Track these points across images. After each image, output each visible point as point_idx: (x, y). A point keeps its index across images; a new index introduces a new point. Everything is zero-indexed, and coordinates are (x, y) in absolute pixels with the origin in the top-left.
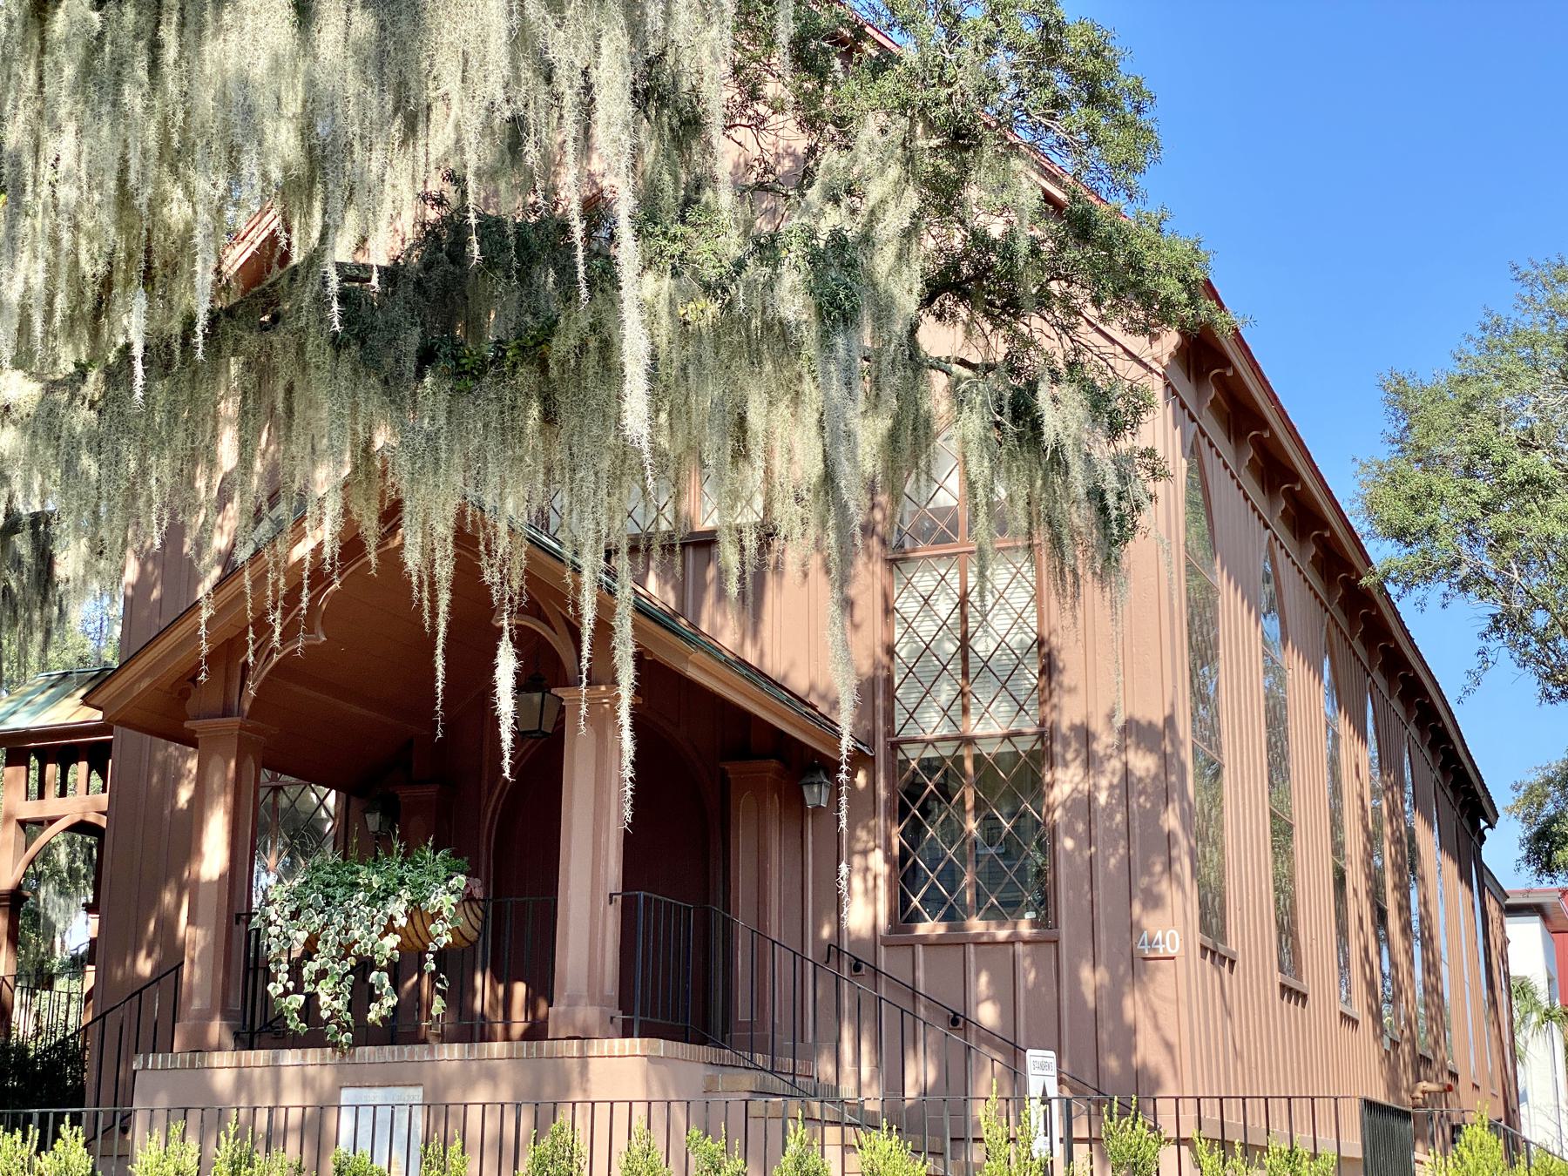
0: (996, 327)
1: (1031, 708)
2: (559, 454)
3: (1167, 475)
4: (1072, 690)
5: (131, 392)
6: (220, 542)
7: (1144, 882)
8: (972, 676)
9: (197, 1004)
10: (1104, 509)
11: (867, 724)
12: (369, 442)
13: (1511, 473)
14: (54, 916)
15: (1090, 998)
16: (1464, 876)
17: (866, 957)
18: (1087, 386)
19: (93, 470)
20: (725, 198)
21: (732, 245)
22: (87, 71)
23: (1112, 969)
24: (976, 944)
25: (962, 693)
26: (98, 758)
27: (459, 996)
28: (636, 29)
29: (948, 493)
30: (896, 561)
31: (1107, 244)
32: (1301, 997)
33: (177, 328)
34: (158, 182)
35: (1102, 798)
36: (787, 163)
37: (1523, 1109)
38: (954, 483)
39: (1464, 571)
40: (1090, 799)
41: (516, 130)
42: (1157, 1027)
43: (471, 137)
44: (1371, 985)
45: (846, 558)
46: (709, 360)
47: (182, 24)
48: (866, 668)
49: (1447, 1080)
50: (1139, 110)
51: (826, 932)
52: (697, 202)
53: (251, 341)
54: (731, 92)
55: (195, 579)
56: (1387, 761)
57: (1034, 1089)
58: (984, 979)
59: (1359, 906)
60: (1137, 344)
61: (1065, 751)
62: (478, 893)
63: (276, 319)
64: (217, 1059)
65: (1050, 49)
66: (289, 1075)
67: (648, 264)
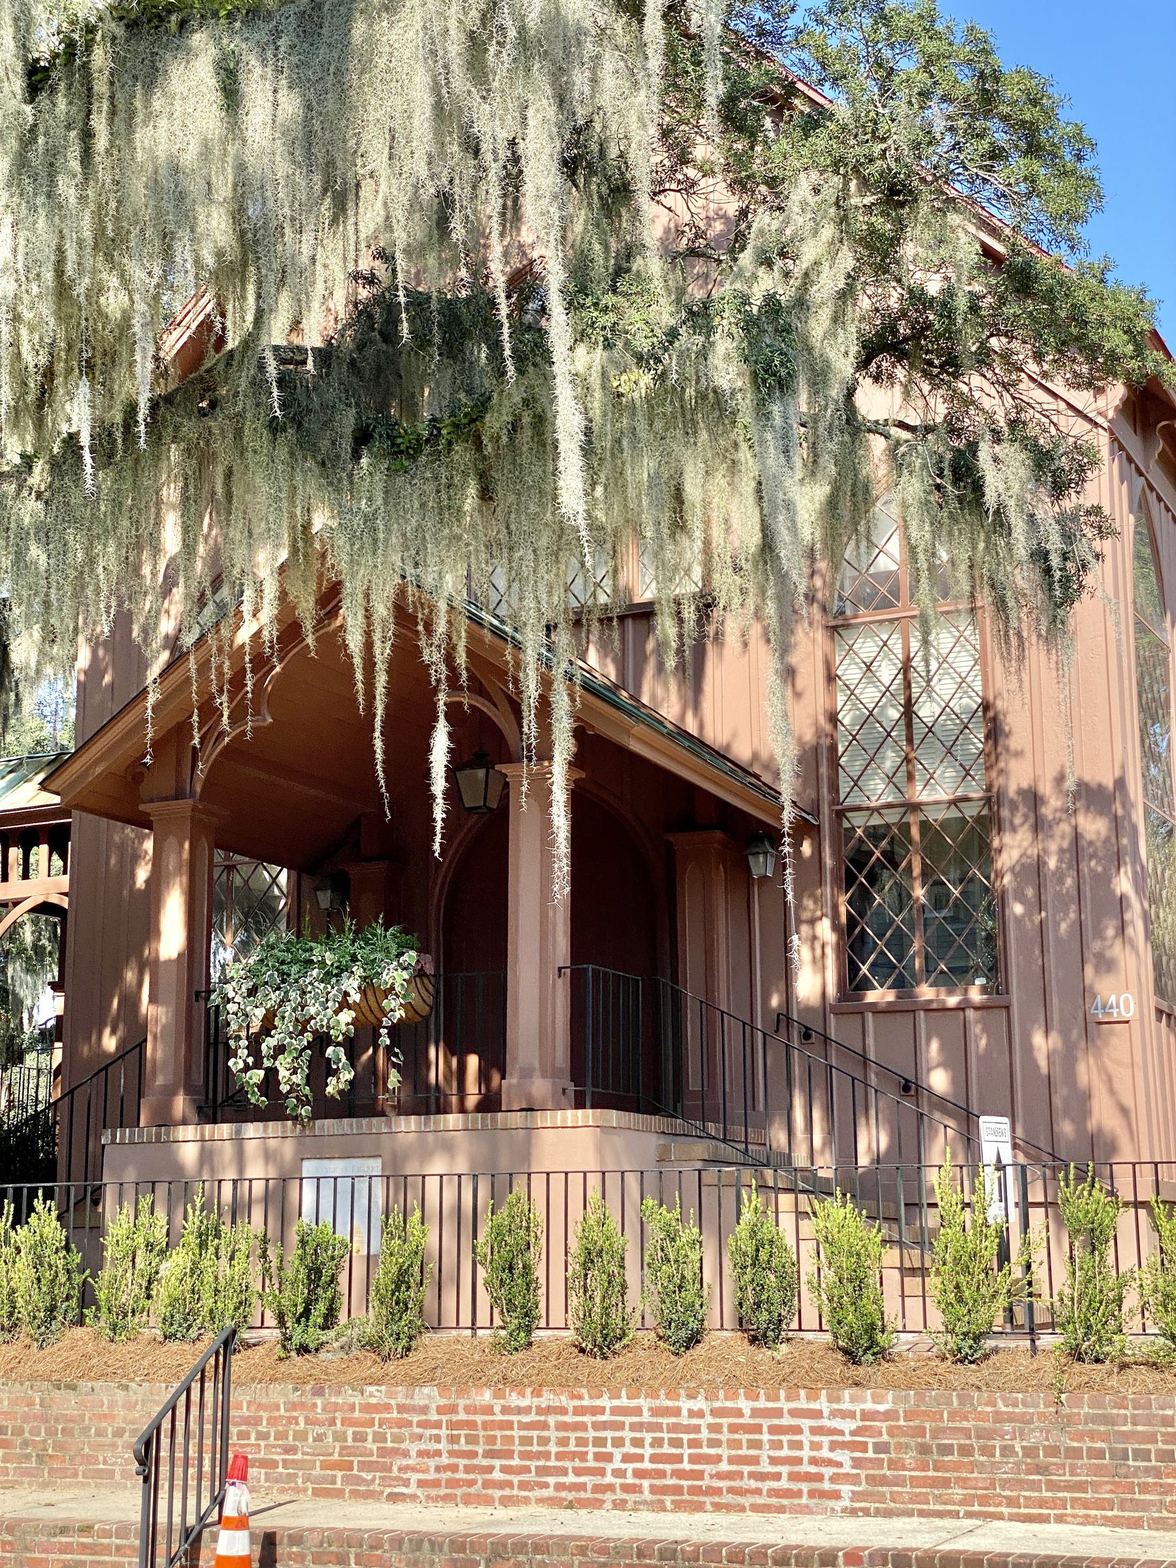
1: (978, 773)
3: (1114, 533)
4: (1019, 754)
6: (167, 626)
7: (1096, 946)
8: (916, 742)
9: (160, 1081)
10: (1048, 571)
11: (811, 793)
12: (307, 526)
14: (22, 992)
15: (1043, 1063)
20: (652, 265)
21: (665, 314)
23: (1065, 1033)
24: (926, 1010)
25: (907, 760)
26: (58, 840)
27: (415, 1068)
30: (838, 626)
31: (1049, 297)
34: (95, 271)
35: (1052, 863)
36: (718, 226)
38: (894, 547)
40: (1040, 863)
42: (1112, 1092)
46: (642, 426)
47: (113, 113)
48: (809, 736)
50: (1079, 158)
51: (775, 1001)
53: (190, 427)
54: (661, 157)
55: (144, 665)
58: (935, 1045)
60: (1082, 398)
61: (1012, 814)
62: (430, 969)
63: (213, 405)
64: (188, 1132)
66: (251, 1147)
67: (581, 336)
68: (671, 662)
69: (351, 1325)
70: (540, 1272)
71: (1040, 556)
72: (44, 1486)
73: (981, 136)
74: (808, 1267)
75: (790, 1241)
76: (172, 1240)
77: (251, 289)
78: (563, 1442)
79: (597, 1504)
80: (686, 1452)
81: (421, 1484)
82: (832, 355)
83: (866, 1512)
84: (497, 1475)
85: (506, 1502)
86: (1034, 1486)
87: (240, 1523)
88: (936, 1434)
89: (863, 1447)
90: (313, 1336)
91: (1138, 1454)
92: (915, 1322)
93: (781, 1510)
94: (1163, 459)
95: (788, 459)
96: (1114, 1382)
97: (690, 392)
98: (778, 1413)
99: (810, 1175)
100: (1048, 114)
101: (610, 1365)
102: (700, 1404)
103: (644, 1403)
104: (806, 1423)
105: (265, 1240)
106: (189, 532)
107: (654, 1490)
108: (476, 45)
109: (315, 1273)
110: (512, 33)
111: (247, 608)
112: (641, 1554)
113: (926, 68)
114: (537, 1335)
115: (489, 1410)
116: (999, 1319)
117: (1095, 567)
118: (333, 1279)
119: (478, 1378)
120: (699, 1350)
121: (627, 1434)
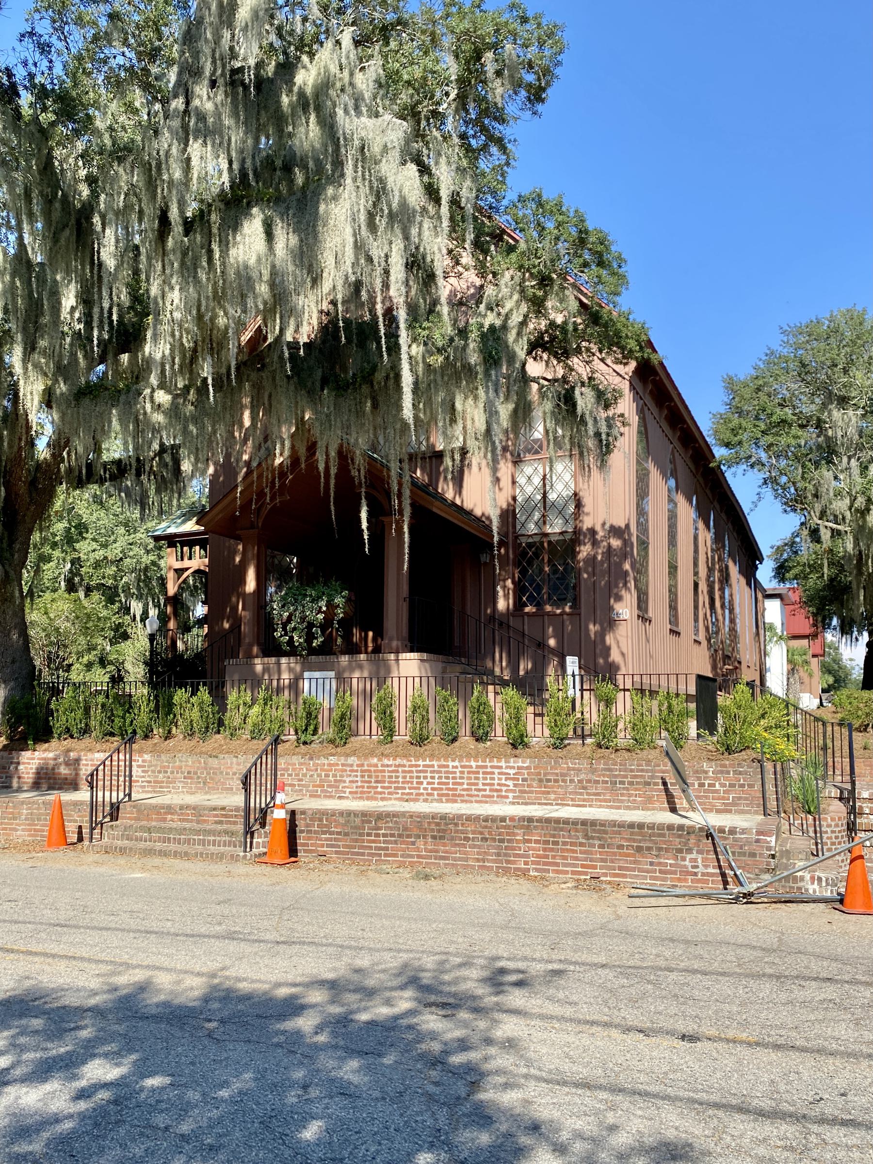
0: (559, 362)
1: (571, 522)
2: (379, 420)
3: (629, 425)
4: (588, 514)
5: (209, 399)
6: (246, 457)
7: (615, 591)
9: (247, 640)
10: (601, 441)
11: (505, 529)
12: (303, 417)
13: (774, 418)
14: (189, 604)
15: (593, 636)
16: (749, 584)
17: (505, 621)
18: (595, 388)
19: (195, 431)
20: (445, 310)
21: (449, 330)
22: (183, 264)
25: (544, 516)
26: (203, 544)
27: (347, 636)
28: (407, 237)
29: (538, 433)
30: (517, 462)
31: (606, 326)
32: (678, 634)
33: (224, 370)
34: (214, 309)
35: (599, 557)
36: (472, 291)
37: (768, 674)
38: (541, 428)
39: (753, 460)
41: (357, 286)
42: (619, 647)
43: (339, 288)
44: (707, 628)
45: (495, 461)
46: (439, 379)
47: (220, 241)
48: (505, 506)
49: (736, 664)
50: (620, 267)
51: (489, 611)
52: (434, 311)
53: (254, 376)
54: (448, 261)
55: (236, 474)
56: (718, 539)
57: (569, 671)
58: (551, 629)
59: (704, 598)
60: (619, 368)
62: (353, 598)
63: (263, 366)
64: (258, 661)
65: (581, 243)
66: (284, 667)
67: (414, 340)
68: (449, 477)
69: (323, 733)
70: (396, 715)
71: (598, 434)
72: (206, 793)
73: (580, 256)
74: (498, 713)
75: (492, 703)
76: (254, 701)
77: (278, 316)
78: (404, 777)
79: (416, 800)
80: (451, 781)
81: (350, 793)
82: (517, 350)
83: (518, 803)
84: (379, 790)
85: (383, 799)
86: (581, 794)
87: (283, 806)
88: (545, 775)
89: (518, 779)
90: (309, 738)
91: (621, 783)
92: (539, 733)
93: (486, 802)
94: (651, 392)
95: (497, 394)
96: (613, 756)
97: (459, 364)
98: (486, 767)
99: (501, 679)
100: (607, 248)
101: (422, 749)
102: (456, 763)
103: (435, 763)
104: (496, 771)
105: (290, 702)
106: (254, 418)
107: (438, 795)
108: (371, 216)
109: (309, 714)
110: (386, 212)
111: (278, 451)
112: (433, 818)
113: (557, 228)
114: (395, 738)
115: (376, 766)
116: (571, 733)
117: (621, 440)
118: (316, 717)
119: (372, 754)
120: (457, 744)
121: (429, 775)
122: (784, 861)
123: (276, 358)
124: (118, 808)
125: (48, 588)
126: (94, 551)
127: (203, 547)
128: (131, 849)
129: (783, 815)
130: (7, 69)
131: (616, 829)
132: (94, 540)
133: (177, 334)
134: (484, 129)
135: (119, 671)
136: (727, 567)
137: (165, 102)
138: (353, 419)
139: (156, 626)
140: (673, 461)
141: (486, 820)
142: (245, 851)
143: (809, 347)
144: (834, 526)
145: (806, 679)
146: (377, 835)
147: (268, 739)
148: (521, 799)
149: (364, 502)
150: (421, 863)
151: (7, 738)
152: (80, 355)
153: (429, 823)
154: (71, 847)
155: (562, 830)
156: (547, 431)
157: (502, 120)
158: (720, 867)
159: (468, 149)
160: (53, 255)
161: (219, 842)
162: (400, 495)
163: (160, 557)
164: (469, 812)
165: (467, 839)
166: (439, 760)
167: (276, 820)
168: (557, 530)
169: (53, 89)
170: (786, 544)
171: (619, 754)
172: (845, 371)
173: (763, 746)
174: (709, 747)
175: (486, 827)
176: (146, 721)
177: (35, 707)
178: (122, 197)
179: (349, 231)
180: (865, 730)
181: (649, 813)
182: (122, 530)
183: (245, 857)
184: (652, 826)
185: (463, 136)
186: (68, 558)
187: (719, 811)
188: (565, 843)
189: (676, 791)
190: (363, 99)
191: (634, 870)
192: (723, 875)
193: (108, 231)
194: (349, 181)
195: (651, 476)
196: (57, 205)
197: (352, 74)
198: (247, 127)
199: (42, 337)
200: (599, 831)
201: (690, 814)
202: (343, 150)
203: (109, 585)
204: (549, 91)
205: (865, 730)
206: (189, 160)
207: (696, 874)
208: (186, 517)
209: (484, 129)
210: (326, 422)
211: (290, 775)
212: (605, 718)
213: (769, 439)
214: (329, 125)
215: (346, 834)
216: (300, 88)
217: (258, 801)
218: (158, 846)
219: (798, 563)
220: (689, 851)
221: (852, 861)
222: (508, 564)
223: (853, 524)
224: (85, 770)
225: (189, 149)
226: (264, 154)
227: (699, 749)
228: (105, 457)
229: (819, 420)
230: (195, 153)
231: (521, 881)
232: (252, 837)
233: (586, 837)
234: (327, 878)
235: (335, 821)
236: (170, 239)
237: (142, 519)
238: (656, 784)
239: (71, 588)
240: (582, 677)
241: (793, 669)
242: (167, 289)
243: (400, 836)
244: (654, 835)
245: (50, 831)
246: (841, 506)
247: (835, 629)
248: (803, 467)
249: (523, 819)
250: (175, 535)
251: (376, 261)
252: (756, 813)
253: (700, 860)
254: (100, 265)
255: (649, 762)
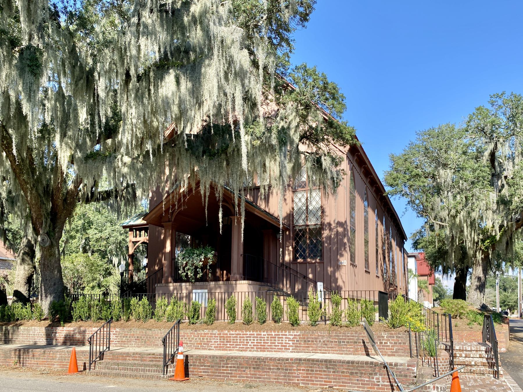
0: (314, 145)
1: (320, 219)
3: (346, 174)
4: (327, 216)
6: (167, 189)
7: (340, 252)
9: (166, 275)
10: (334, 181)
12: (194, 169)
13: (413, 173)
15: (329, 273)
16: (401, 250)
18: (331, 157)
19: (142, 175)
21: (263, 129)
22: (136, 96)
23: (334, 268)
25: (307, 217)
26: (146, 230)
27: (214, 273)
28: (243, 85)
29: (304, 178)
30: (294, 192)
32: (369, 273)
34: (151, 118)
35: (333, 236)
36: (273, 113)
38: (305, 176)
39: (403, 192)
40: (330, 236)
42: (342, 279)
44: (382, 271)
47: (154, 86)
48: (288, 212)
50: (343, 100)
53: (170, 150)
54: (262, 98)
55: (162, 196)
56: (387, 229)
57: (319, 289)
58: (310, 270)
59: (380, 256)
60: (341, 148)
62: (217, 254)
64: (171, 284)
66: (183, 287)
67: (247, 133)
68: (263, 197)
69: (202, 319)
70: (236, 310)
72: (146, 347)
73: (324, 96)
74: (285, 309)
75: (282, 304)
76: (169, 303)
78: (240, 340)
79: (246, 351)
84: (228, 346)
85: (230, 350)
86: (324, 347)
87: (182, 353)
89: (294, 341)
90: (195, 321)
93: (279, 351)
96: (339, 329)
98: (279, 335)
99: (287, 293)
100: (337, 91)
102: (265, 333)
103: (255, 333)
104: (284, 337)
105: (186, 304)
107: (256, 348)
109: (195, 310)
110: (233, 72)
112: (254, 359)
114: (236, 321)
115: (227, 334)
116: (319, 319)
118: (198, 311)
119: (225, 329)
120: (265, 324)
121: (252, 339)
122: (421, 379)
123: (181, 141)
124: (103, 354)
125: (74, 251)
126: (96, 234)
127: (146, 231)
128: (109, 374)
129: (419, 357)
130: (54, 4)
131: (341, 364)
132: (96, 229)
133: (134, 129)
134: (279, 34)
135: (107, 290)
136: (391, 242)
137: (128, 20)
138: (217, 170)
139: (124, 269)
140: (366, 194)
141: (279, 360)
142: (164, 374)
143: (429, 141)
144: (441, 223)
145: (427, 295)
146: (227, 367)
147: (175, 321)
148: (296, 349)
149: (221, 209)
150: (248, 380)
151: (51, 321)
152: (88, 140)
153: (252, 361)
154: (80, 373)
155: (315, 364)
156: (308, 177)
157: (288, 30)
158: (390, 382)
159: (272, 44)
160: (76, 92)
161: (152, 370)
162: (239, 205)
163: (127, 237)
164: (271, 356)
165: (270, 369)
166: (257, 331)
167: (179, 360)
168: (313, 223)
169: (75, 14)
170: (418, 232)
171: (342, 328)
172: (446, 152)
173: (410, 325)
174: (385, 325)
175: (279, 363)
176: (118, 313)
177: (64, 306)
178: (108, 64)
179: (215, 81)
180: (456, 318)
181: (356, 356)
182: (109, 224)
183: (164, 377)
184: (358, 363)
185: (270, 38)
186: (84, 237)
187: (389, 355)
188: (316, 371)
189: (369, 346)
190: (223, 19)
191: (349, 383)
192: (392, 386)
193: (101, 79)
194: (215, 57)
195: (356, 199)
196: (77, 69)
197: (217, 7)
198: (167, 32)
199: (69, 130)
200: (333, 365)
201: (376, 357)
202: (213, 42)
203: (103, 250)
204: (310, 15)
205: (456, 318)
206: (139, 46)
207: (378, 385)
208: (139, 216)
209: (279, 34)
210: (205, 171)
211: (185, 339)
212: (336, 312)
213: (410, 183)
214: (206, 31)
215: (212, 367)
216: (193, 13)
217: (170, 351)
218: (122, 372)
219: (424, 241)
220: (376, 374)
221: (453, 379)
222: (290, 239)
223: (450, 223)
224: (88, 336)
225: (140, 41)
226: (176, 45)
227: (380, 326)
228: (100, 189)
229: (433, 174)
230: (143, 43)
231: (296, 389)
232: (167, 368)
233: (327, 368)
234: (203, 388)
235: (207, 360)
236: (131, 84)
237: (118, 219)
238: (359, 343)
239: (85, 251)
240: (325, 292)
241: (420, 290)
242: (129, 108)
243: (238, 367)
244: (359, 367)
245: (70, 366)
246: (444, 214)
247: (440, 271)
248: (427, 196)
249: (297, 359)
250: (133, 226)
251: (228, 95)
252: (407, 356)
253: (380, 379)
254: (98, 95)
255: (356, 332)
